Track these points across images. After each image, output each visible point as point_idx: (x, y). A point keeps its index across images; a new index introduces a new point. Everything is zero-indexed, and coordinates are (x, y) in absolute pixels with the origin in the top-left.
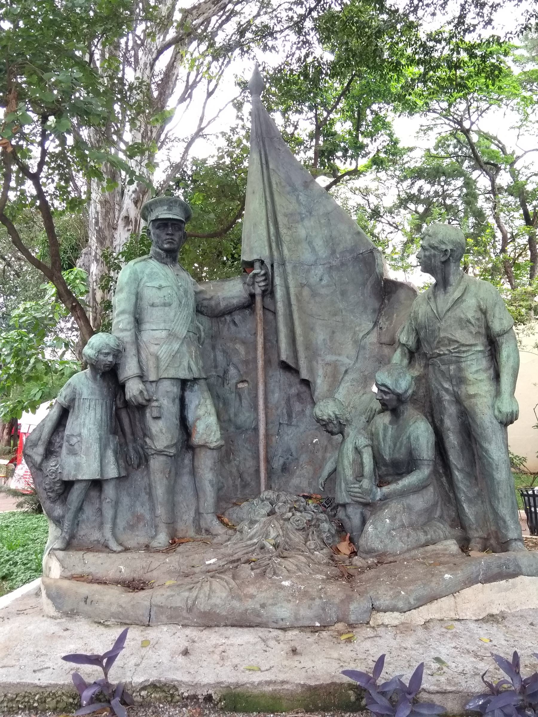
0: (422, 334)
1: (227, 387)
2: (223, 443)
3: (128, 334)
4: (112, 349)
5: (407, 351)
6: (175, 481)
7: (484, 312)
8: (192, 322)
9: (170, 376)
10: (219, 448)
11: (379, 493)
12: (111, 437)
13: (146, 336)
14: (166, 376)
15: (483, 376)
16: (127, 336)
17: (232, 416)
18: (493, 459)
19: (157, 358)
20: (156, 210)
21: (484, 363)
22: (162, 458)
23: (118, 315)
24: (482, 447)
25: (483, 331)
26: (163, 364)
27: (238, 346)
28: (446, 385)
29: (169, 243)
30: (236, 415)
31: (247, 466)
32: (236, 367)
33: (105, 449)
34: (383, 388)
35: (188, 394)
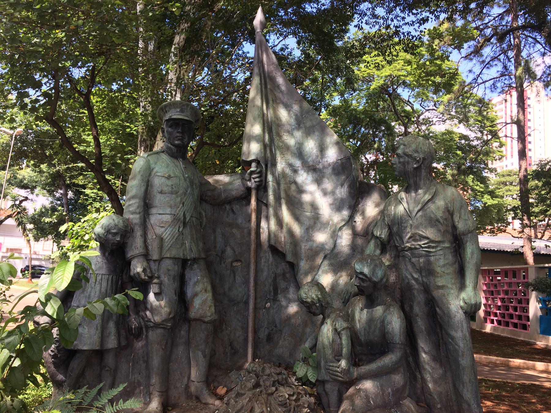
0: (395, 229)
1: (223, 265)
2: (216, 317)
3: (138, 216)
4: (119, 229)
5: (379, 243)
6: (171, 351)
7: (452, 214)
8: (195, 208)
9: (172, 256)
10: (212, 322)
11: (356, 372)
13: (154, 219)
14: (168, 256)
15: (450, 270)
16: (135, 218)
17: (226, 289)
18: (459, 346)
19: (162, 240)
20: (170, 112)
22: (159, 331)
23: (129, 199)
24: (448, 335)
25: (450, 229)
26: (166, 245)
27: (234, 231)
28: (416, 276)
29: (179, 140)
30: (230, 289)
31: (237, 335)
32: (233, 249)
33: (108, 321)
34: (361, 276)
35: (188, 274)
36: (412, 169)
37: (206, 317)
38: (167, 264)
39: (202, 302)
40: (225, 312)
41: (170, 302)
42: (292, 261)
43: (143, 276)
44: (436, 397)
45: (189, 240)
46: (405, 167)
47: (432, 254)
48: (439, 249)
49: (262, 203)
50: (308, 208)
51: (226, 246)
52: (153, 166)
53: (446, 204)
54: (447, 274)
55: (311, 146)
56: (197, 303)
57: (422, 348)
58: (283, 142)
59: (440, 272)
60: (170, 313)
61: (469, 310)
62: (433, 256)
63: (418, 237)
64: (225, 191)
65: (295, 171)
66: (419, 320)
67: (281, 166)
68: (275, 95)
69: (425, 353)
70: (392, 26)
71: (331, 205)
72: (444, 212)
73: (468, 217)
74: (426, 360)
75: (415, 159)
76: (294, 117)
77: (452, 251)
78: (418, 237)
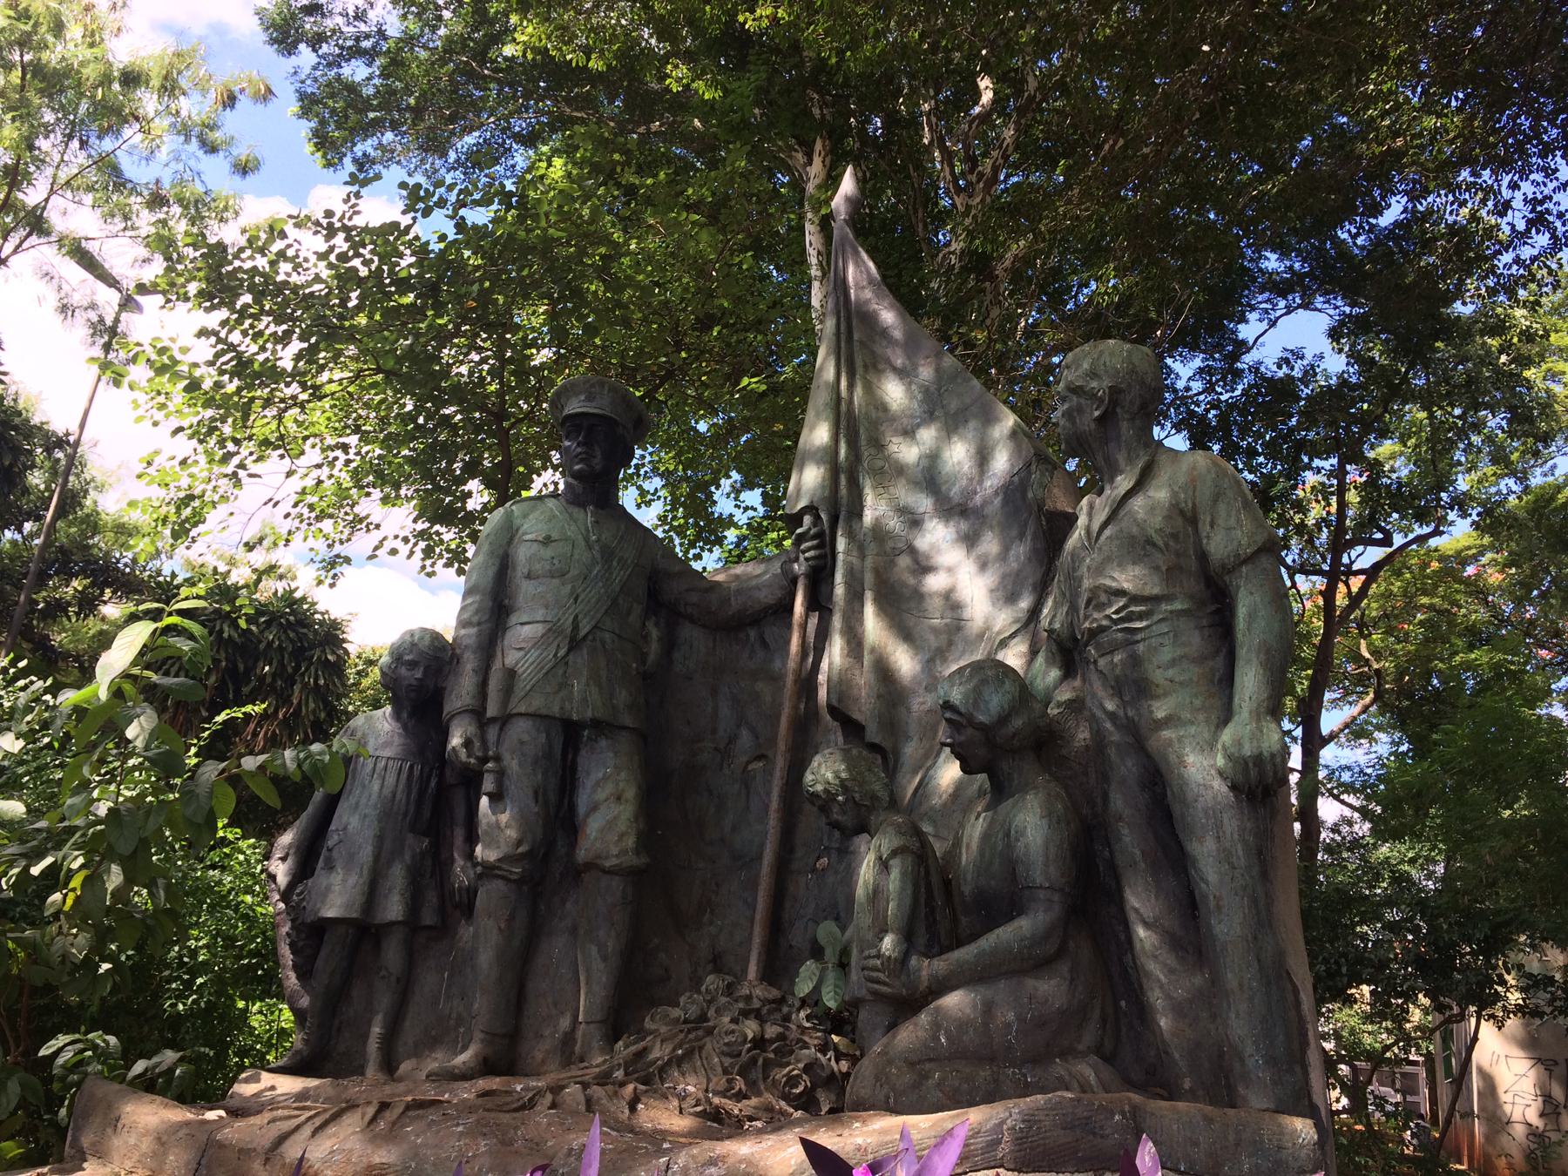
7: (1192, 519)
9: (531, 710)
10: (634, 875)
11: (927, 968)
12: (410, 839)
14: (522, 709)
21: (1195, 641)
25: (1193, 564)
26: (522, 686)
29: (581, 461)
30: (734, 829)
32: (753, 730)
33: (389, 863)
35: (584, 759)
36: (1093, 426)
37: (607, 858)
38: (520, 730)
39: (608, 819)
40: (717, 885)
41: (523, 821)
42: (877, 741)
43: (463, 754)
44: (1177, 1056)
45: (584, 680)
46: (1074, 423)
47: (1139, 637)
48: (1156, 618)
49: (819, 602)
50: (935, 604)
51: (738, 726)
52: (517, 522)
53: (1174, 494)
54: (1181, 683)
55: (958, 454)
56: (593, 827)
57: (1136, 911)
58: (888, 458)
59: (1161, 681)
60: (519, 843)
61: (1240, 778)
62: (1143, 640)
63: (1103, 598)
64: (739, 592)
65: (915, 522)
66: (1126, 831)
67: (874, 508)
68: (873, 353)
69: (1147, 925)
70: (1518, 203)
71: (992, 591)
72: (1168, 518)
73: (1238, 520)
74: (1148, 946)
75: (1092, 395)
76: (920, 396)
77: (1205, 622)
78: (1103, 598)
